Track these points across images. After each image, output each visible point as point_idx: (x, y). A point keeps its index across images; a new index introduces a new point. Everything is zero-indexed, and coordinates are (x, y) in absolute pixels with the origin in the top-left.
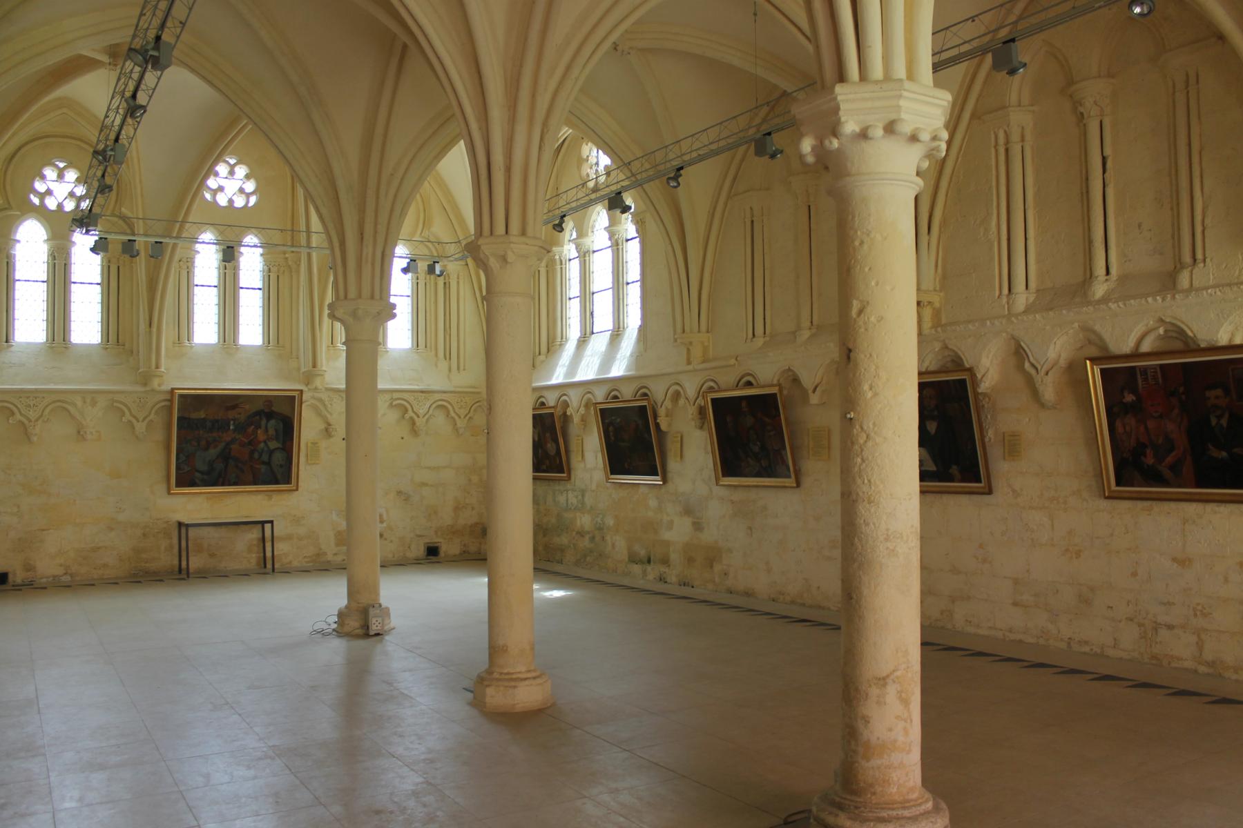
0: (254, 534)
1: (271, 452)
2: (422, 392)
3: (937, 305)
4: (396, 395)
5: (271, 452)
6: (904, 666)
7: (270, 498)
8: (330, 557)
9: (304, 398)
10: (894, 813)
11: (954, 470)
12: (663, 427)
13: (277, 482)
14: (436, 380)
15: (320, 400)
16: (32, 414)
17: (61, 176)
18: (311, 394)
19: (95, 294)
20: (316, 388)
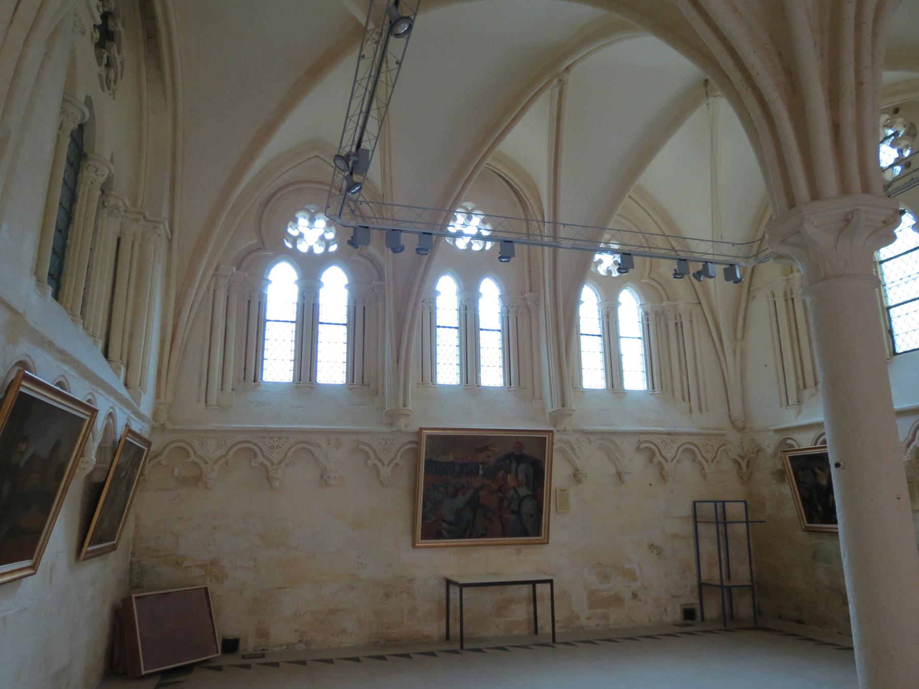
1: (521, 500)
2: (669, 434)
5: (521, 500)
14: (681, 421)
15: (569, 443)
16: (276, 457)
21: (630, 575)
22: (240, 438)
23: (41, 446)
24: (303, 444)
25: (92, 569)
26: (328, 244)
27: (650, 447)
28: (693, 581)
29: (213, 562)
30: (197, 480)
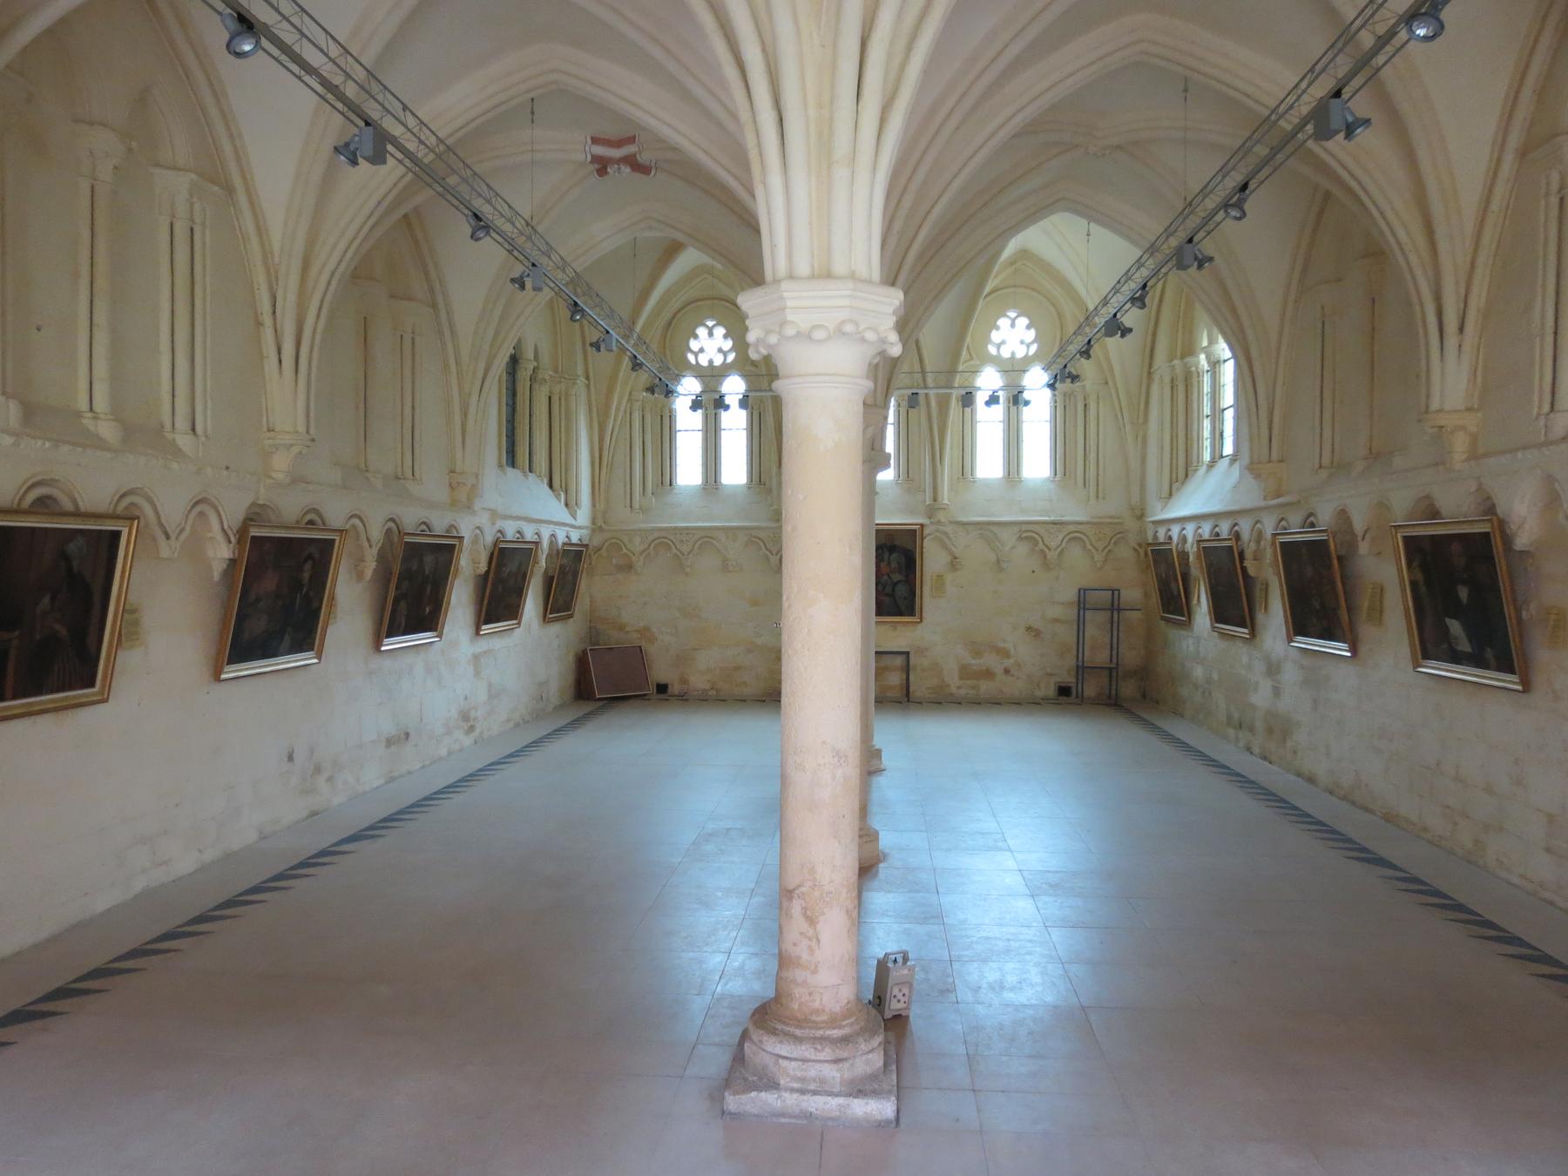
0: (899, 661)
1: (895, 584)
2: (1054, 523)
3: (1473, 429)
4: (1024, 528)
5: (895, 584)
6: (810, 883)
7: (895, 629)
8: (953, 689)
9: (926, 531)
10: (787, 1029)
11: (1489, 654)
12: (1252, 572)
13: (901, 614)
14: (1074, 512)
15: (945, 533)
16: (685, 549)
17: (711, 334)
18: (933, 528)
19: (742, 438)
20: (939, 522)
21: (1003, 653)
22: (656, 534)
23: (512, 567)
24: (705, 539)
25: (555, 628)
26: (725, 354)
27: (1029, 533)
28: (1070, 661)
29: (647, 629)
30: (628, 567)
